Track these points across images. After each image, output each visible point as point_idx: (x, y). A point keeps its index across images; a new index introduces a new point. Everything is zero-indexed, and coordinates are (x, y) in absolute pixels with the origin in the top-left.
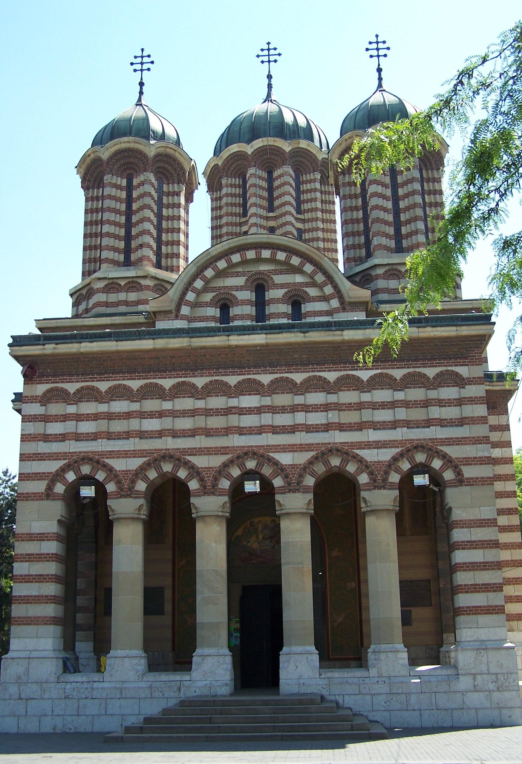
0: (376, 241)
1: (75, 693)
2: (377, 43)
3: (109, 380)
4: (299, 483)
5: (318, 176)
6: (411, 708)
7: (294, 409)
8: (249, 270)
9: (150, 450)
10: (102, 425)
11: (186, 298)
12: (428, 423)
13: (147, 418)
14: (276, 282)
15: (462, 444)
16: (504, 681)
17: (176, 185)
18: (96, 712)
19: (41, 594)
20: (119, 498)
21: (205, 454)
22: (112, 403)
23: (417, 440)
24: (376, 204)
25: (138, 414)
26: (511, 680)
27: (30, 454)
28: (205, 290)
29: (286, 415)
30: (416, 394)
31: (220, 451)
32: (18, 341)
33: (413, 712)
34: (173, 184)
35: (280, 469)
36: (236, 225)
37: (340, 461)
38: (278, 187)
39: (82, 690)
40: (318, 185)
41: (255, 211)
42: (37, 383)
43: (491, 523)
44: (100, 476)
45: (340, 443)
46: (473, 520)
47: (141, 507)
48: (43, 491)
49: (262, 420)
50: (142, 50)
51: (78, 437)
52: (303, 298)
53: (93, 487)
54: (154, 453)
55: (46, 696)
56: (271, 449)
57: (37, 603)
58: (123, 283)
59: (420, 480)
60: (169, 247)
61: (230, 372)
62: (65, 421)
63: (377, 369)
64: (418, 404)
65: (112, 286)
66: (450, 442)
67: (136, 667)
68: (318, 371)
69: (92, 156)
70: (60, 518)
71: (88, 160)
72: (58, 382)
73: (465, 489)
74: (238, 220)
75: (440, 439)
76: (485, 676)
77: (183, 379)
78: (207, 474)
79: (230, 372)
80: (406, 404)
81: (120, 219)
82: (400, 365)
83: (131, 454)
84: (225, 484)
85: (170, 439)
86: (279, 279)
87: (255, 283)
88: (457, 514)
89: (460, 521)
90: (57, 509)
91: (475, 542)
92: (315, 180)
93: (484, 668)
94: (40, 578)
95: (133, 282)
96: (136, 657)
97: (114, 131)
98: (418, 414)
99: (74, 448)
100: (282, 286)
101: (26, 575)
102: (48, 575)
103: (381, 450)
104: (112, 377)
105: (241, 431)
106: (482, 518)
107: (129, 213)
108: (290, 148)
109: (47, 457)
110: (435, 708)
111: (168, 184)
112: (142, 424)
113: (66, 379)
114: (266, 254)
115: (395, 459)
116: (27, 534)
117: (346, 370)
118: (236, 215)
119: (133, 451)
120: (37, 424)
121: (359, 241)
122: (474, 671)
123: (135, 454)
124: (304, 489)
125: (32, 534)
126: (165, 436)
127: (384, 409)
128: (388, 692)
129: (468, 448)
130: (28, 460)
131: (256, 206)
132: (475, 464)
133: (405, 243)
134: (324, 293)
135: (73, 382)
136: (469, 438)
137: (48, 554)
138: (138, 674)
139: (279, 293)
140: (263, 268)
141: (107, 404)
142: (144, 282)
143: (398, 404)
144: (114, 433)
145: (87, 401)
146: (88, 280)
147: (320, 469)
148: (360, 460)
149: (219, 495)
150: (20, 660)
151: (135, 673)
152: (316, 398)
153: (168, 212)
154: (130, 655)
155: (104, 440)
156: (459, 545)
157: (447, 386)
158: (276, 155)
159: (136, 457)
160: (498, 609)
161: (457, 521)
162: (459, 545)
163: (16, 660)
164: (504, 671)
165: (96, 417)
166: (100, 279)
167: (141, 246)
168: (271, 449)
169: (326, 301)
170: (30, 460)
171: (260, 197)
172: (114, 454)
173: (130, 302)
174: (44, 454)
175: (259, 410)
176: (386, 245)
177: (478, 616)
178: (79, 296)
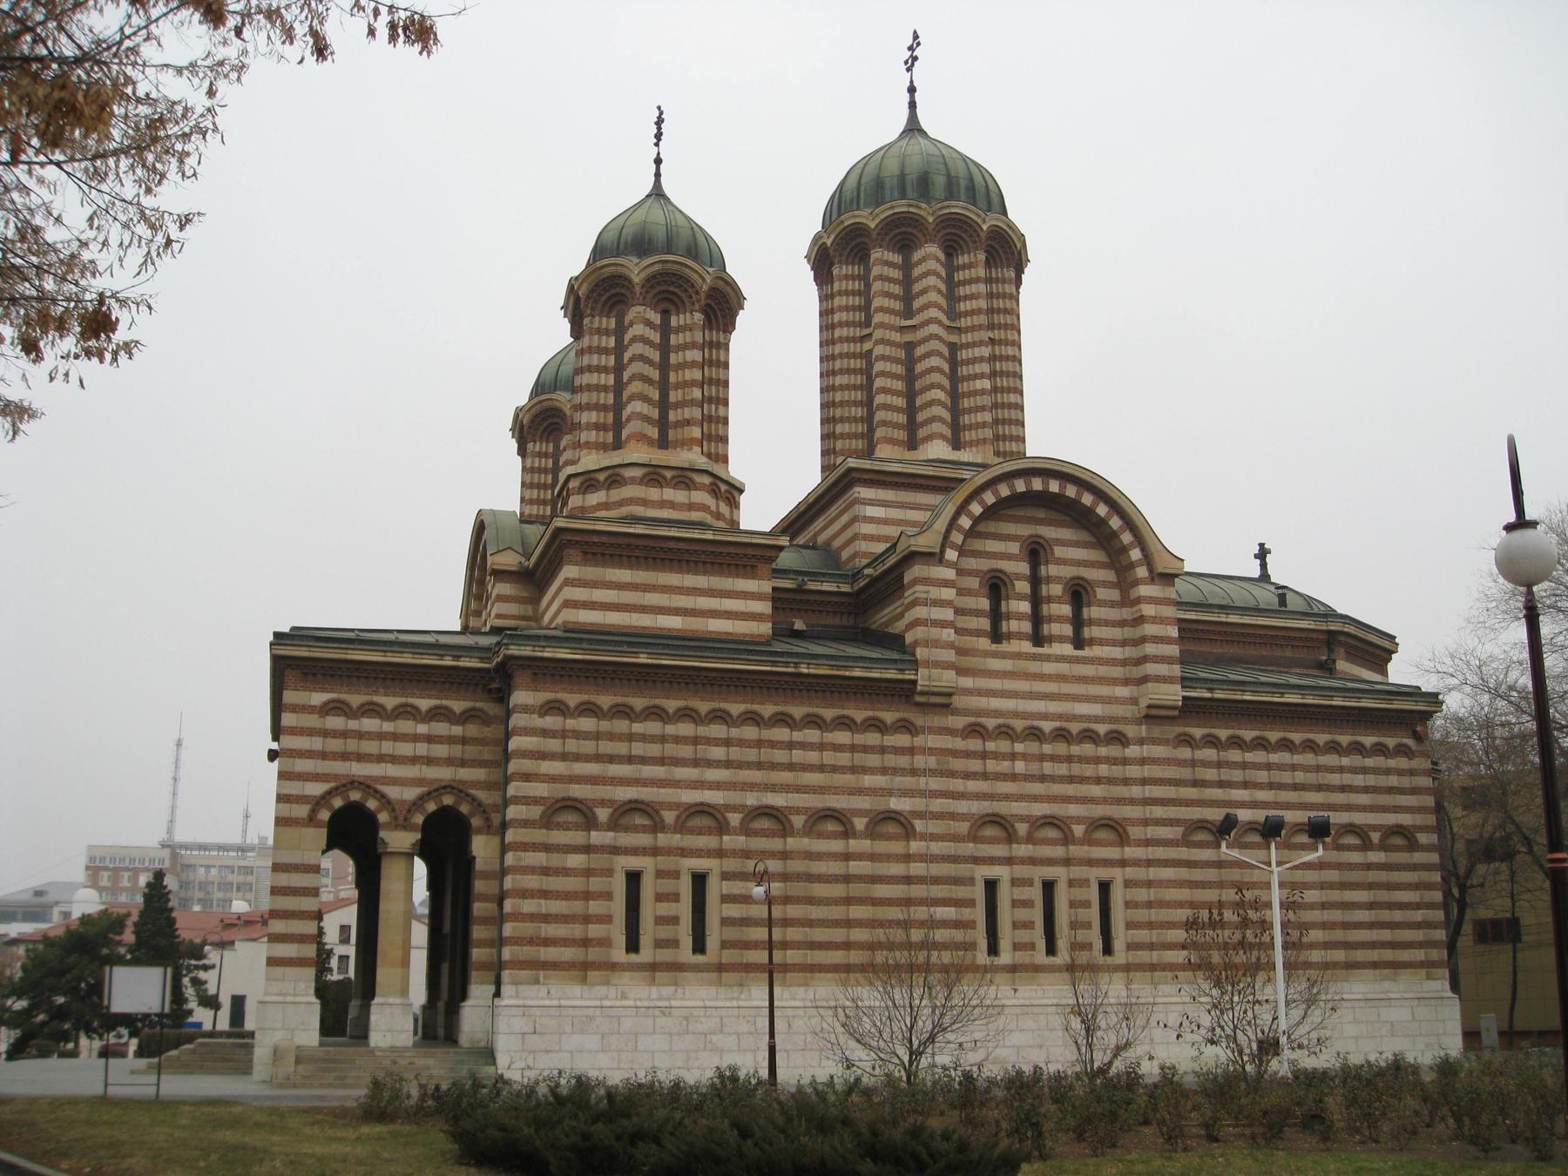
5: (982, 257)
36: (854, 340)
58: (669, 474)
115: (329, 793)
142: (699, 478)
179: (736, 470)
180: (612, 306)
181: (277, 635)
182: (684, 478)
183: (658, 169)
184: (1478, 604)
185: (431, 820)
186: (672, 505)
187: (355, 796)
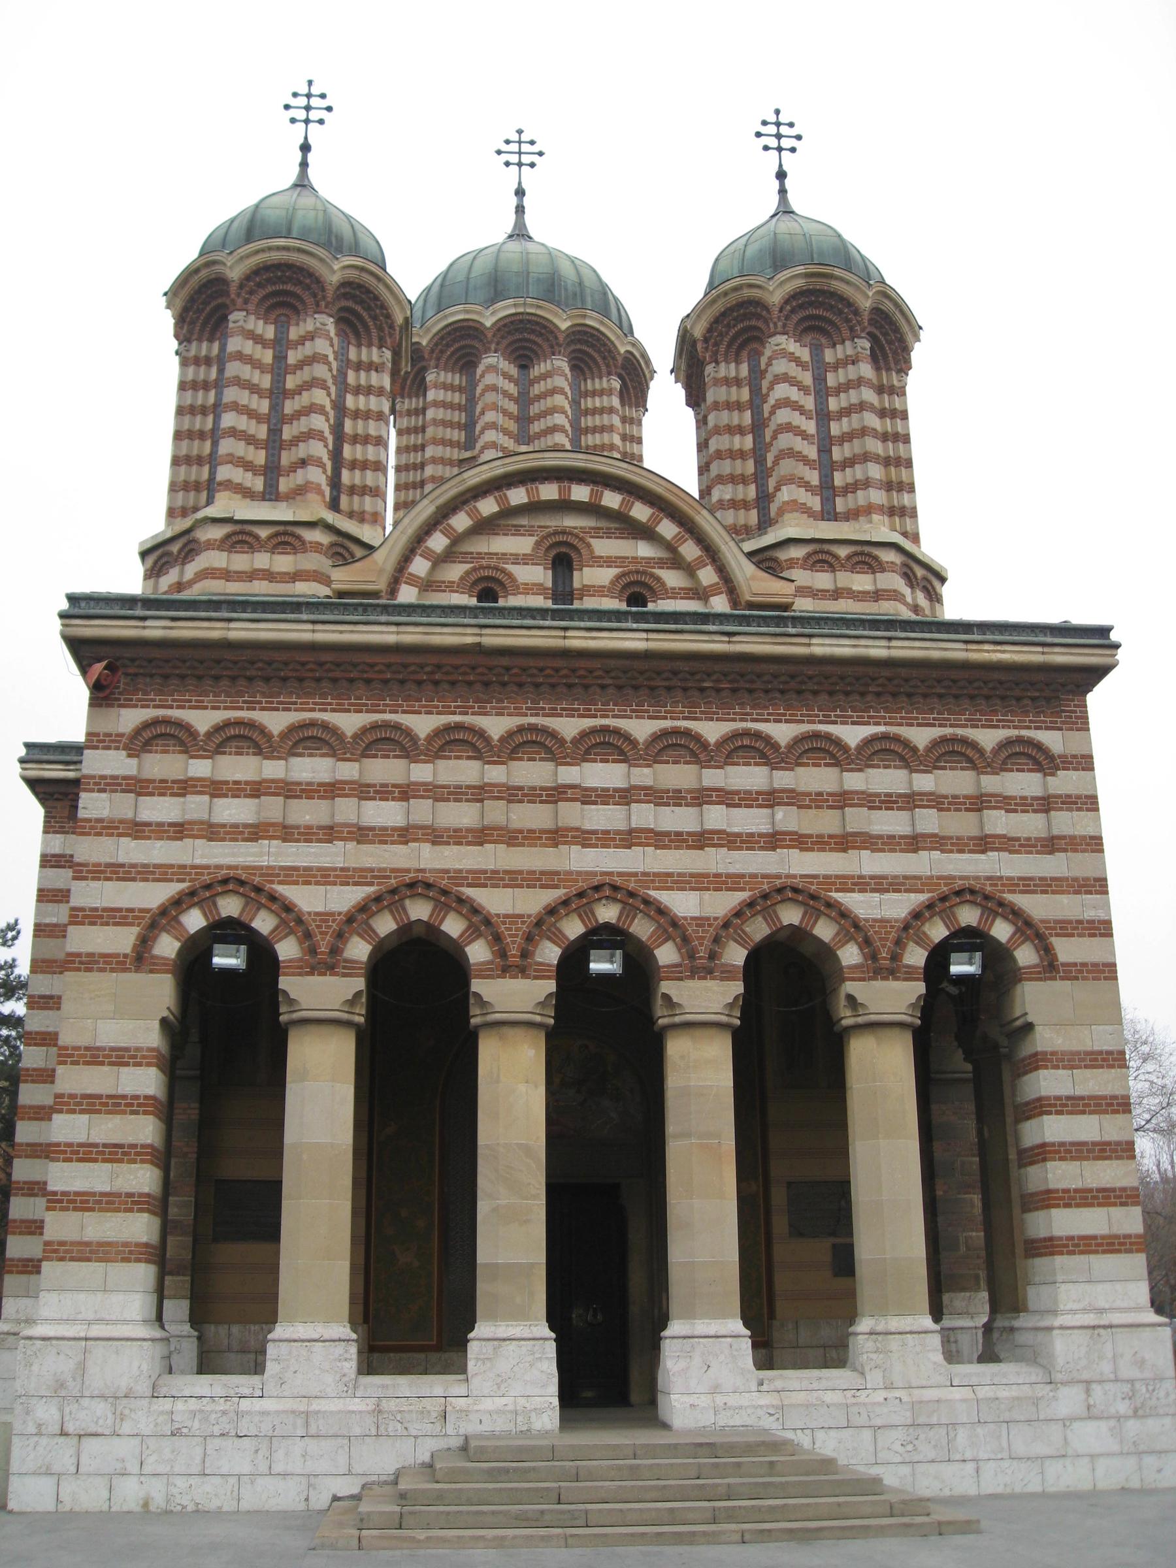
0: (786, 494)
1: (196, 1424)
2: (778, 124)
3: (289, 710)
4: (713, 956)
6: (958, 1457)
7: (701, 797)
8: (542, 524)
9: (380, 870)
10: (273, 808)
11: (410, 570)
12: (984, 843)
13: (374, 799)
14: (597, 553)
15: (1054, 892)
16: (1148, 1395)
17: (375, 350)
18: (246, 1469)
19: (114, 1190)
20: (308, 974)
21: (505, 886)
22: (295, 761)
23: (962, 878)
24: (788, 421)
25: (354, 789)
26: (1162, 1394)
27: (99, 865)
28: (448, 556)
29: (684, 809)
30: (956, 781)
31: (539, 880)
32: (81, 606)
33: (962, 1465)
34: (370, 345)
35: (671, 926)
37: (800, 916)
38: (539, 398)
39: (214, 1416)
40: (616, 402)
41: (494, 438)
42: (120, 706)
43: (1114, 1060)
44: (263, 923)
45: (802, 876)
46: (1078, 1053)
47: (358, 995)
48: (128, 950)
49: (633, 818)
50: (310, 83)
51: (212, 832)
52: (650, 588)
53: (243, 948)
54: (389, 877)
55: (126, 1428)
56: (653, 881)
57: (108, 1210)
58: (263, 533)
59: (227, 959)
60: (357, 472)
61: (562, 709)
62: (184, 795)
63: (878, 724)
64: (960, 803)
65: (241, 536)
66: (1028, 885)
67: (339, 1364)
68: (753, 720)
69: (204, 273)
70: (166, 1013)
71: (195, 281)
72: (171, 707)
73: (1060, 986)
74: (456, 454)
75: (1008, 878)
76: (1107, 1386)
77: (458, 718)
78: (510, 929)
79: (562, 709)
80: (938, 802)
81: (259, 404)
82: (923, 719)
83: (336, 876)
84: (550, 953)
85: (426, 849)
86: (603, 547)
87: (553, 553)
88: (1046, 1039)
89: (1053, 1053)
90: (160, 993)
91: (1082, 1098)
92: (610, 392)
93: (1106, 1368)
94: (115, 1153)
95: (285, 533)
96: (340, 1340)
97: (252, 226)
98: (962, 824)
99: (202, 857)
100: (609, 562)
101: (81, 1145)
102: (134, 1146)
103: (887, 896)
104: (295, 703)
105: (586, 838)
106: (1096, 1048)
107: (278, 394)
108: (568, 324)
109: (139, 873)
110: (1005, 1455)
111: (359, 346)
112: (362, 810)
113: (190, 701)
114: (580, 493)
116: (87, 1049)
117: (814, 722)
118: (451, 444)
119: (342, 869)
120: (118, 796)
121: (745, 494)
122: (1086, 1376)
123: (347, 877)
124: (722, 972)
125: (98, 1049)
126: (415, 840)
127: (892, 809)
128: (909, 1421)
129: (1064, 899)
130: (94, 879)
131: (497, 429)
132: (1080, 935)
133: (840, 504)
134: (698, 581)
135: (206, 708)
136: (1067, 879)
137: (137, 1097)
138: (346, 1379)
139: (603, 576)
140: (570, 522)
141: (283, 762)
143: (922, 800)
144: (298, 827)
145: (237, 754)
146: (187, 523)
147: (759, 930)
148: (843, 915)
149: (536, 978)
150: (66, 1342)
151: (338, 1378)
152: (749, 777)
153: (357, 402)
154: (326, 1337)
155: (275, 842)
156: (1050, 1105)
157: (1018, 770)
158: (541, 335)
159: (348, 884)
160: (1131, 1244)
161: (1045, 1053)
162: (1050, 1105)
163: (54, 1342)
164: (1148, 1374)
165: (256, 790)
166: (215, 521)
167: (303, 463)
168: (653, 881)
169: (699, 599)
170: (99, 879)
171: (505, 412)
172: (298, 876)
173: (278, 573)
174: (133, 866)
175: (625, 796)
176: (805, 504)
177: (1092, 1256)
178: (158, 556)
179: (931, 548)
180: (741, 347)
181: (72, 599)
182: (865, 557)
183: (782, 185)
184: (1151, 1039)
185: (756, 958)
186: (269, 576)
187: (419, 910)
